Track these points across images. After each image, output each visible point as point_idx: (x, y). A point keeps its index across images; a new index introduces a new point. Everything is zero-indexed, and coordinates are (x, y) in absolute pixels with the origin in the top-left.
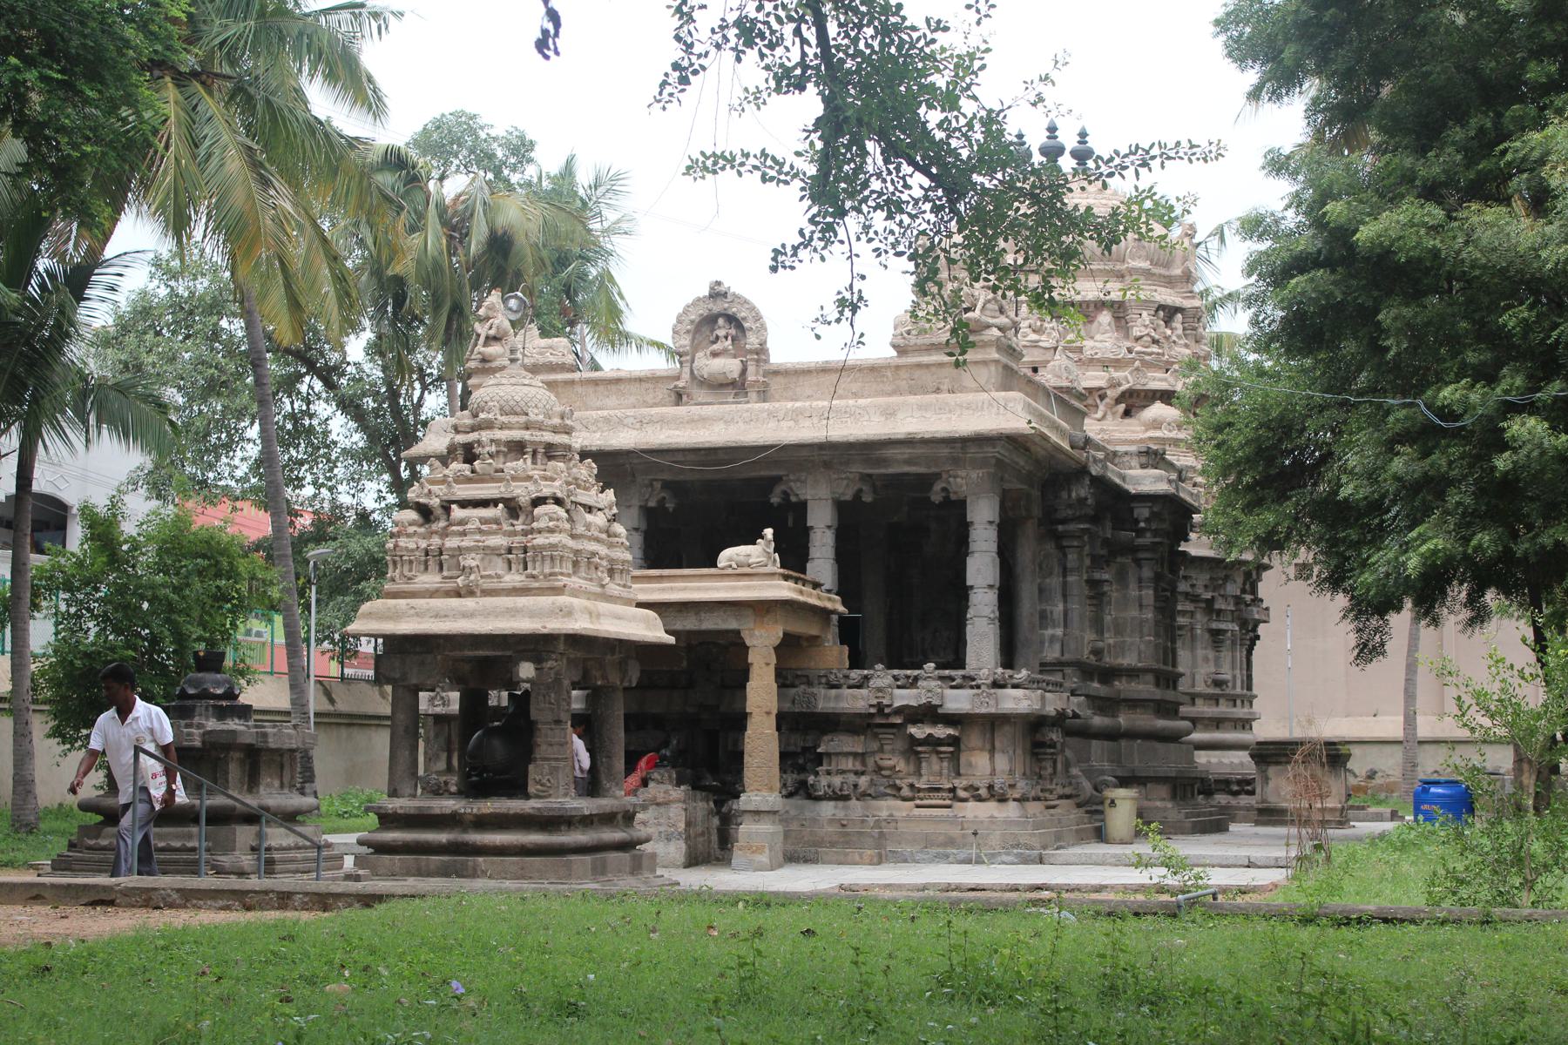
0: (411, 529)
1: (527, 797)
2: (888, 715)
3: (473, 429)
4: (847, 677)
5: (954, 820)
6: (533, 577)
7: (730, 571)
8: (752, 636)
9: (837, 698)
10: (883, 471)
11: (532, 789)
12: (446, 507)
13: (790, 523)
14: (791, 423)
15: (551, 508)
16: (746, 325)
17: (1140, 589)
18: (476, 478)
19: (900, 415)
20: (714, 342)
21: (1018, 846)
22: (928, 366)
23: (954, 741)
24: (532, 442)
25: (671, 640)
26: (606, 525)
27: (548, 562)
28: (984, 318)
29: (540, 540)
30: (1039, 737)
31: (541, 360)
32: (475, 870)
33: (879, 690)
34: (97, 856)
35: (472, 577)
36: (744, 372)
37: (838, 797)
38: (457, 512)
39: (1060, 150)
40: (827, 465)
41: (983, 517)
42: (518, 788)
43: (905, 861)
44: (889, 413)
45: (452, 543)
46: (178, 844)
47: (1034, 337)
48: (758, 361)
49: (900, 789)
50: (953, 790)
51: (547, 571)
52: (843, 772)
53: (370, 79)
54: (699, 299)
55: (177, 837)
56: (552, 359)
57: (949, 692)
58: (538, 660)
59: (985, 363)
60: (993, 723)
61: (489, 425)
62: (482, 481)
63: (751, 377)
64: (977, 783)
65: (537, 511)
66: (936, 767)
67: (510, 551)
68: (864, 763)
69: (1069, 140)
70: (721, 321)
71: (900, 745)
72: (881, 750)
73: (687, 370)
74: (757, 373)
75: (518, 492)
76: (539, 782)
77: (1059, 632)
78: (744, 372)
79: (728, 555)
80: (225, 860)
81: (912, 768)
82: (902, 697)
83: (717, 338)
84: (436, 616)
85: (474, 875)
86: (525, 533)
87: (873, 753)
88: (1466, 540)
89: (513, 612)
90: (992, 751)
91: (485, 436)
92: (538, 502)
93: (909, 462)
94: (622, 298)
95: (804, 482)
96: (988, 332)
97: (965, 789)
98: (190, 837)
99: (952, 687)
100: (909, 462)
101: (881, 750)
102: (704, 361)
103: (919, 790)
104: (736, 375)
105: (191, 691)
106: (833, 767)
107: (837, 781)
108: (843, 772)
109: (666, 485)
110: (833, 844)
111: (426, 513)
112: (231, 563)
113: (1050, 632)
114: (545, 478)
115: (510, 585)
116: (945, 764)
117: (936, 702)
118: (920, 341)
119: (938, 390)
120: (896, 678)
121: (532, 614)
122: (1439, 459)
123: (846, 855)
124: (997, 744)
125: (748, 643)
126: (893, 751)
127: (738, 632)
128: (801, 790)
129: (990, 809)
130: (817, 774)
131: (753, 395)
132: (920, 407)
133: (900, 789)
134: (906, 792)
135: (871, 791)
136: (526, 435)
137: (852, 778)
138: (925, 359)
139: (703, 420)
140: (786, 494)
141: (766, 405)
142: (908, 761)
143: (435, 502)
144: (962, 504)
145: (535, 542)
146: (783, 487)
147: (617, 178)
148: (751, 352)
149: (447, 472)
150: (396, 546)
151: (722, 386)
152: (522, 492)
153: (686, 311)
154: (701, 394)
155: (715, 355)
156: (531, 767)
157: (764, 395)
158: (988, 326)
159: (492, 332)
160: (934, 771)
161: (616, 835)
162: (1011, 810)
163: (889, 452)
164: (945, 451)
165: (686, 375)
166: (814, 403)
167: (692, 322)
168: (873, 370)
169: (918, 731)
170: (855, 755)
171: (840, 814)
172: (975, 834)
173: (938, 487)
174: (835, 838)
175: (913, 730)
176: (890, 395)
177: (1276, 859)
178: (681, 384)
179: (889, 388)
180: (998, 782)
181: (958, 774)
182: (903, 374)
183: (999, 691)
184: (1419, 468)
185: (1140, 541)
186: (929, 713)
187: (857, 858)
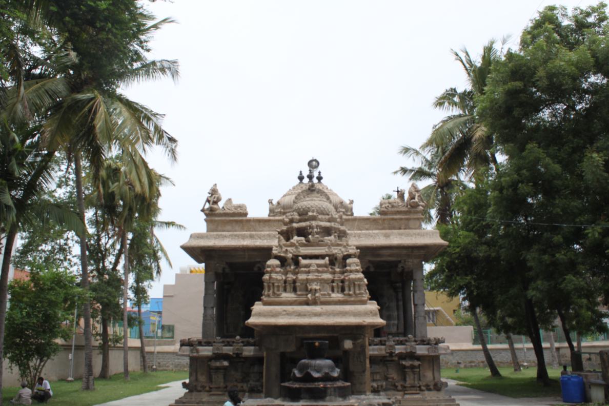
3: (300, 221)
6: (349, 295)
12: (296, 260)
18: (309, 244)
19: (391, 237)
22: (395, 219)
31: (236, 211)
33: (391, 346)
35: (317, 295)
38: (303, 262)
44: (387, 236)
45: (302, 277)
50: (420, 387)
53: (137, 104)
56: (241, 211)
58: (354, 338)
61: (314, 218)
64: (429, 384)
67: (333, 281)
75: (335, 251)
77: (396, 322)
82: (398, 349)
89: (344, 314)
91: (314, 223)
97: (424, 386)
113: (392, 322)
117: (414, 351)
118: (393, 209)
119: (400, 229)
121: (355, 314)
134: (399, 388)
138: (395, 217)
150: (270, 277)
159: (215, 200)
164: (404, 252)
169: (407, 363)
173: (400, 266)
179: (380, 227)
181: (420, 380)
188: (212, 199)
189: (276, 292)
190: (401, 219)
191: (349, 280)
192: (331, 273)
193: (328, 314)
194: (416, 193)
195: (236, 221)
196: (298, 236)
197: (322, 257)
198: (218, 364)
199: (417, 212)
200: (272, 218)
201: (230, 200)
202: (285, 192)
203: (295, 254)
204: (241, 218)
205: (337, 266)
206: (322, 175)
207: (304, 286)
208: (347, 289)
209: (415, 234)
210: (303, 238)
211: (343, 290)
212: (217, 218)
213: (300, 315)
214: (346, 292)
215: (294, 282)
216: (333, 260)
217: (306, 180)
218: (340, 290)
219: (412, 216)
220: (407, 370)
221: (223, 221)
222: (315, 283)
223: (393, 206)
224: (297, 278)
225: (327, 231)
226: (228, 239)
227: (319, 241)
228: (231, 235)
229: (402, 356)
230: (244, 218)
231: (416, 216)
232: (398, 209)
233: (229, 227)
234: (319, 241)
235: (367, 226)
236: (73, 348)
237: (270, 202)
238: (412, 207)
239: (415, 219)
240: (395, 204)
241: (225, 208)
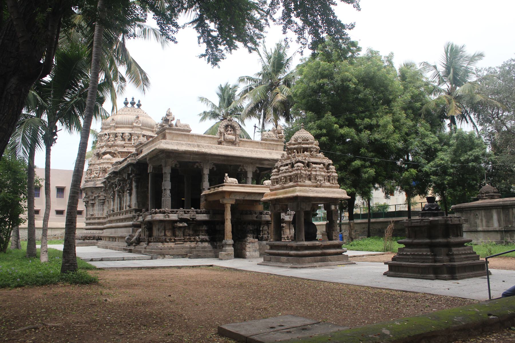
11: (334, 238)
18: (312, 156)
25: (350, 197)
39: (134, 103)
40: (252, 163)
44: (271, 154)
45: (314, 173)
89: (334, 192)
93: (268, 165)
100: (268, 165)
109: (214, 164)
131: (237, 145)
139: (231, 149)
140: (241, 170)
147: (221, 89)
154: (224, 143)
161: (339, 250)
168: (257, 143)
190: (274, 144)
195: (185, 135)
197: (320, 164)
198: (181, 225)
200: (206, 135)
206: (141, 103)
217: (129, 105)
219: (279, 143)
220: (284, 225)
221: (176, 134)
223: (270, 136)
224: (311, 173)
228: (186, 144)
230: (188, 133)
233: (180, 138)
235: (257, 147)
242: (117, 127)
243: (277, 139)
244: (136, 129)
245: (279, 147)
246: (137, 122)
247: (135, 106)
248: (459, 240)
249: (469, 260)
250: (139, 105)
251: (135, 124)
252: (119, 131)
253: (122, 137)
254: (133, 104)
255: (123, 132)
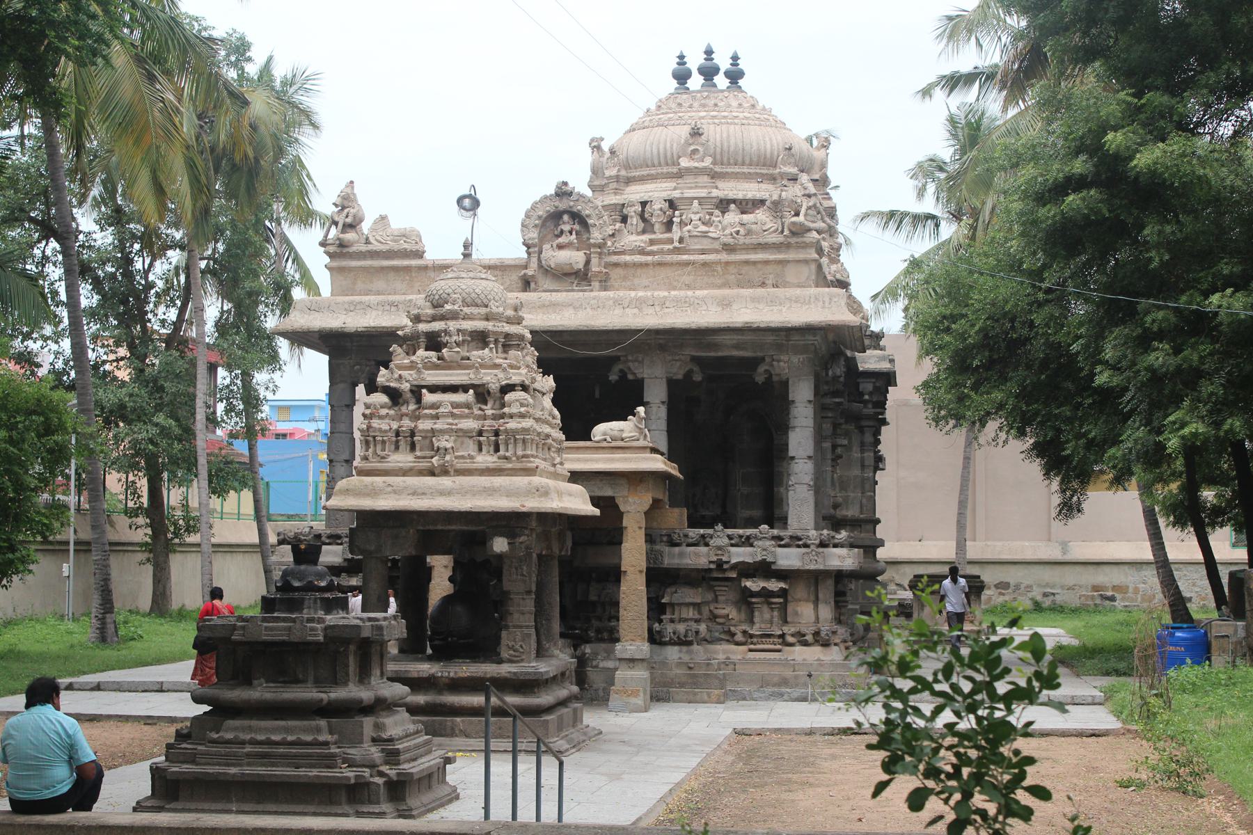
0: (384, 412)
1: (500, 662)
2: (725, 570)
3: (434, 318)
4: (686, 536)
5: (785, 663)
6: (506, 458)
7: (605, 444)
8: (626, 502)
9: (681, 555)
10: (713, 354)
11: (505, 654)
12: (416, 392)
13: (597, 395)
14: (636, 311)
15: (519, 395)
16: (590, 222)
17: (862, 451)
19: (735, 307)
20: (558, 236)
21: (845, 685)
22: (755, 263)
23: (783, 593)
24: (495, 333)
25: (597, 512)
26: (538, 408)
27: (520, 445)
28: (806, 223)
29: (512, 424)
30: (840, 587)
31: (396, 247)
32: (453, 729)
33: (719, 548)
34: (222, 749)
35: (448, 458)
36: (588, 262)
37: (683, 642)
38: (428, 397)
39: (716, 70)
40: (662, 348)
41: (802, 394)
42: (486, 649)
43: (744, 699)
44: (725, 304)
45: (424, 425)
46: (309, 738)
47: (704, 228)
48: (600, 254)
49: (733, 635)
50: (782, 636)
51: (520, 453)
52: (686, 620)
54: (546, 197)
55: (307, 730)
56: (406, 246)
57: (779, 550)
58: (511, 535)
59: (806, 262)
60: (815, 578)
61: (454, 316)
62: (449, 368)
63: (595, 267)
64: (804, 630)
65: (508, 397)
66: (767, 616)
67: (480, 433)
68: (700, 613)
69: (724, 63)
70: (566, 217)
71: (733, 596)
72: (716, 600)
73: (534, 260)
74: (600, 265)
75: (487, 379)
76: (512, 648)
78: (588, 262)
79: (601, 430)
80: (354, 752)
81: (743, 616)
82: (738, 555)
83: (562, 232)
84: (414, 494)
85: (452, 734)
86: (495, 417)
87: (707, 603)
88: (1217, 425)
89: (491, 491)
90: (816, 602)
91: (452, 325)
92: (507, 389)
93: (737, 347)
94: (310, 179)
95: (641, 362)
96: (808, 235)
97: (793, 635)
98: (318, 730)
99: (780, 546)
101: (716, 600)
102: (551, 253)
103: (751, 636)
104: (581, 266)
105: (296, 584)
106: (676, 616)
107: (681, 628)
108: (686, 620)
110: (682, 685)
111: (395, 396)
112: (60, 419)
114: (512, 367)
115: (483, 466)
116: (776, 613)
118: (748, 241)
119: (763, 285)
120: (730, 537)
121: (509, 493)
122: (1191, 356)
123: (695, 694)
124: (821, 596)
125: (622, 508)
126: (726, 602)
127: (613, 498)
128: (655, 639)
129: (812, 654)
130: (660, 621)
131: (596, 284)
132: (753, 299)
133: (733, 635)
134: (739, 637)
135: (708, 637)
136: (489, 326)
137: (694, 626)
139: (554, 305)
140: (623, 374)
141: (611, 294)
142: (739, 610)
143: (406, 386)
144: (785, 384)
145: (508, 426)
146: (621, 366)
148: (595, 245)
149: (413, 358)
151: (566, 275)
152: (493, 379)
153: (533, 208)
154: (547, 283)
155: (560, 247)
156: (504, 634)
157: (605, 284)
158: (809, 230)
159: (349, 220)
160: (764, 619)
162: (834, 654)
163: (719, 338)
164: (770, 338)
165: (534, 264)
166: (656, 293)
167: (540, 217)
169: (753, 585)
170: (694, 605)
171: (686, 658)
172: (810, 676)
173: (761, 369)
174: (684, 679)
175: (749, 584)
176: (720, 287)
177: (1073, 697)
178: (530, 272)
180: (825, 629)
181: (785, 622)
182: (732, 269)
183: (825, 550)
184: (1173, 361)
185: (866, 411)
186: (764, 569)
187: (706, 697)
188: (341, 219)
189: (379, 452)
190: (767, 262)
191: (506, 431)
192: (478, 418)
193: (464, 492)
194: (804, 199)
196: (426, 350)
197: (465, 388)
199: (805, 246)
201: (383, 218)
202: (635, 116)
203: (415, 383)
204: (406, 262)
205: (489, 406)
206: (742, 64)
207: (427, 441)
208: (502, 447)
209: (790, 299)
210: (433, 354)
211: (497, 450)
212: (354, 263)
213: (414, 493)
214: (502, 453)
215: (412, 433)
216: (482, 394)
217: (696, 82)
218: (492, 448)
219: (791, 255)
222: (447, 437)
225: (481, 339)
226: (374, 313)
227: (463, 359)
228: (382, 304)
229: (748, 570)
231: (801, 255)
232: (761, 240)
233: (380, 284)
234: (463, 359)
236: (72, 547)
237: (596, 146)
238: (793, 233)
239: (799, 261)
240: (754, 227)
241: (371, 239)
242: (629, 181)
243: (780, 239)
244: (689, 180)
245: (791, 274)
246: (695, 151)
247: (721, 81)
248: (333, 695)
249: (273, 765)
250: (735, 76)
251: (684, 163)
252: (635, 193)
253: (642, 216)
254: (709, 72)
255: (646, 198)
